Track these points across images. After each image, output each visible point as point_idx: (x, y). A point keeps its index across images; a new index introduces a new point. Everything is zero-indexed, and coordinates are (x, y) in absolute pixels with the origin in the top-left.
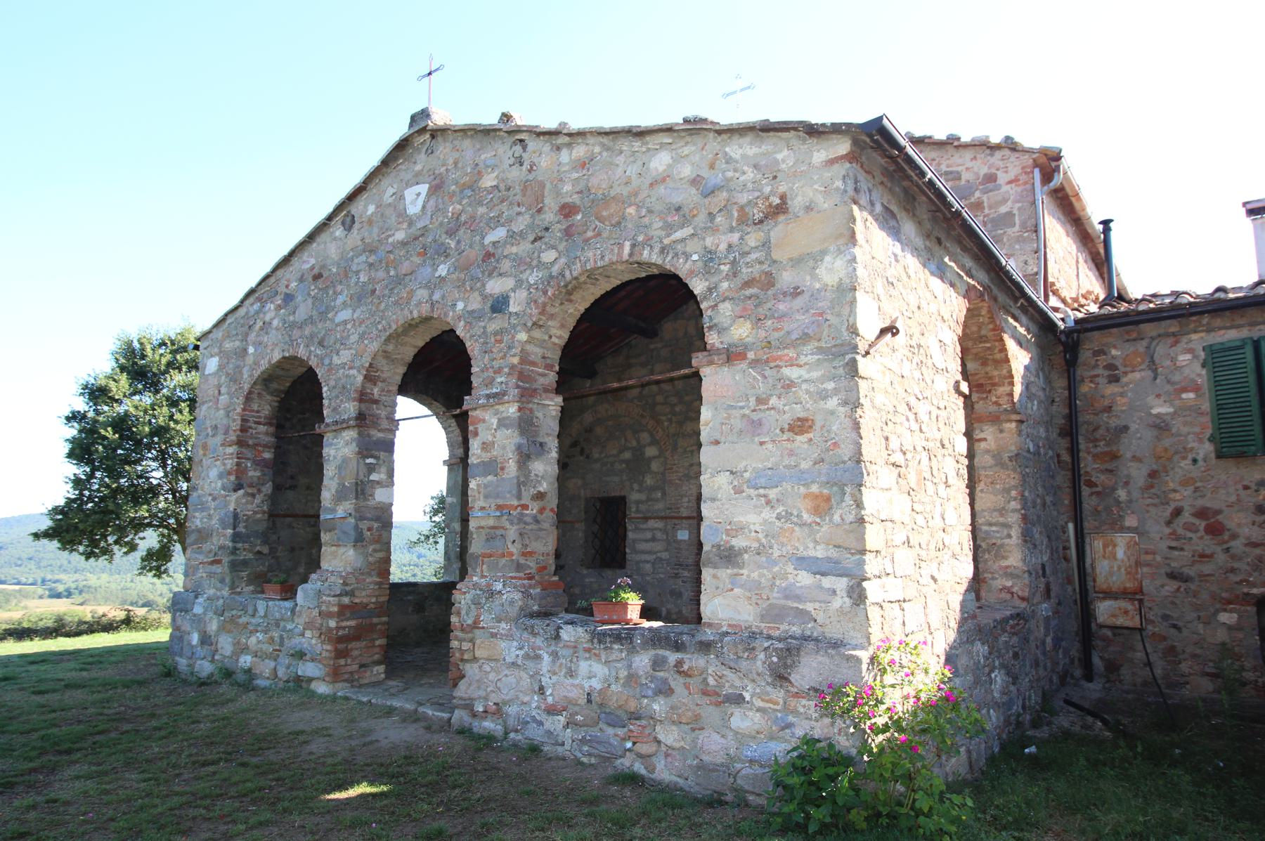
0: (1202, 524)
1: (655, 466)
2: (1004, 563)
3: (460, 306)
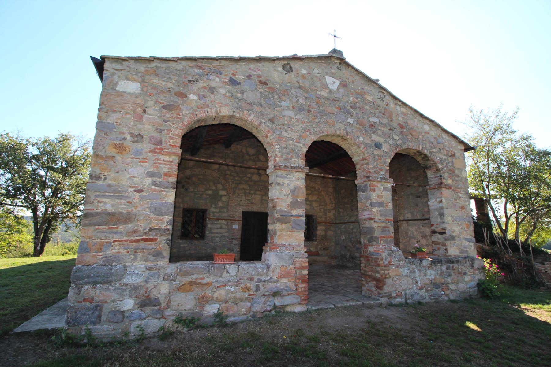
1: (224, 199)
3: (361, 139)
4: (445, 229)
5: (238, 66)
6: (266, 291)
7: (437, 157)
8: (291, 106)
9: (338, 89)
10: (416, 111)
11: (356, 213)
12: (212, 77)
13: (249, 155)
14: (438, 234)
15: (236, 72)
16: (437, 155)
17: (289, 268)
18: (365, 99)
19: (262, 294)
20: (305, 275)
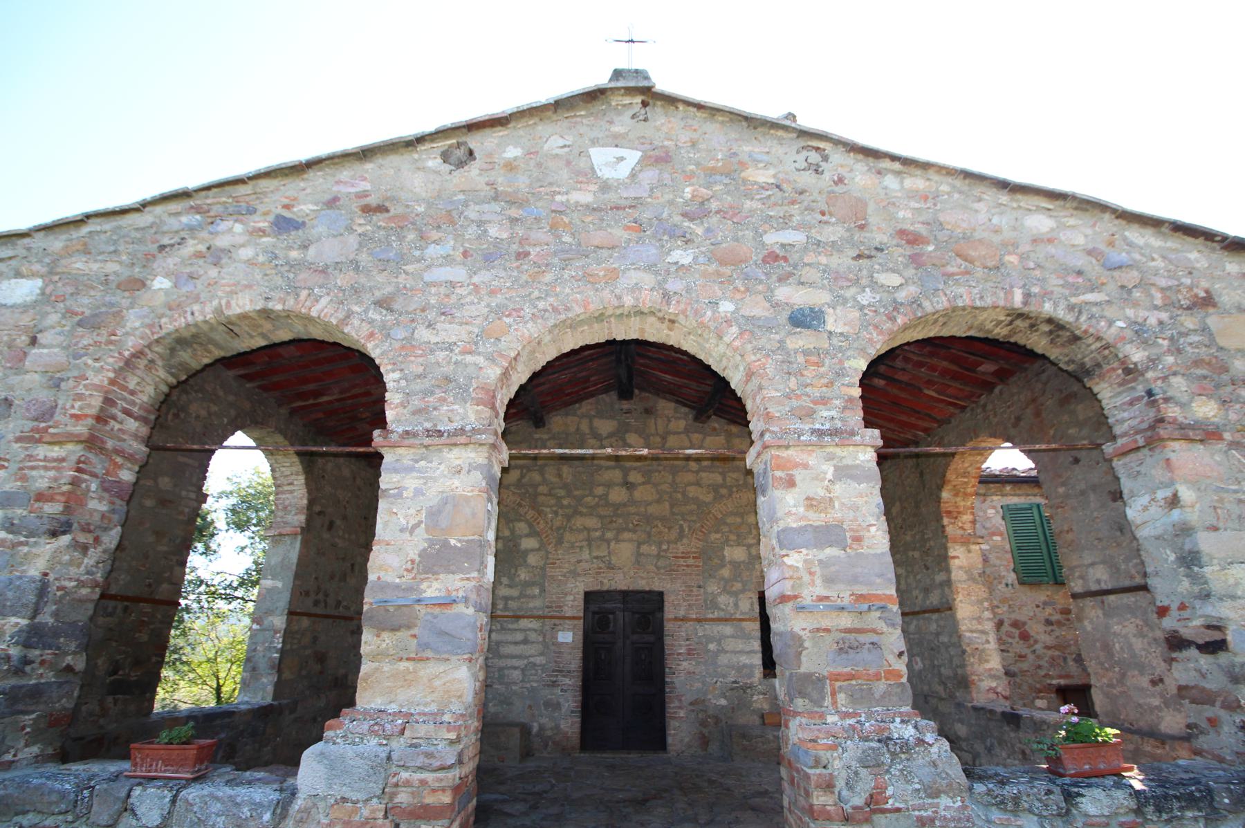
0: (1016, 632)
1: (532, 559)
2: (988, 666)
3: (726, 307)
4: (1218, 628)
5: (302, 184)
7: (1111, 321)
8: (458, 255)
9: (633, 175)
10: (967, 175)
11: (940, 577)
12: (223, 226)
14: (1193, 652)
15: (295, 199)
16: (1109, 312)
17: (366, 812)
18: (745, 181)
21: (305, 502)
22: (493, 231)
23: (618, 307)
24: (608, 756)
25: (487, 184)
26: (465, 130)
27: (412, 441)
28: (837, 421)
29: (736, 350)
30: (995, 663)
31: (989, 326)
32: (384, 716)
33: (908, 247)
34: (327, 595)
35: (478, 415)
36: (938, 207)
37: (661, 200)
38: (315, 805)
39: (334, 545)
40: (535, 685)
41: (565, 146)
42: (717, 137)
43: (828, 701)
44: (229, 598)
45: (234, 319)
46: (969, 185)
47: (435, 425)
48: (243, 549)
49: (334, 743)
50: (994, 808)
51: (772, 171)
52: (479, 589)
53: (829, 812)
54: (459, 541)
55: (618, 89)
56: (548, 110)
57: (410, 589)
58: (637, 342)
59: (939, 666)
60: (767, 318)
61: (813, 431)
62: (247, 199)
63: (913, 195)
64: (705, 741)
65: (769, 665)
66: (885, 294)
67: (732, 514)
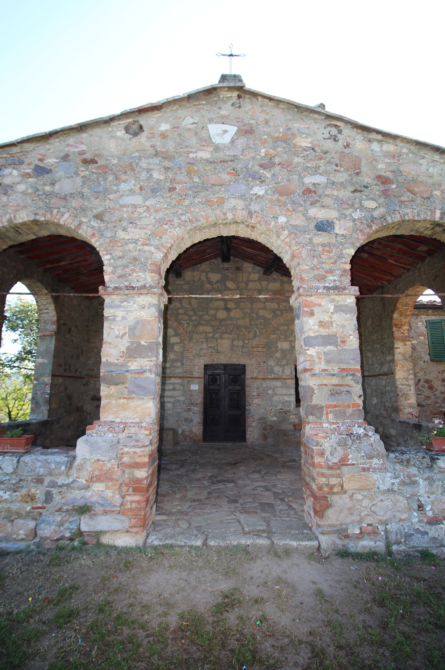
0: (427, 385)
1: (176, 348)
3: (282, 220)
5: (48, 146)
6: (65, 504)
9: (233, 141)
13: (210, 283)
15: (45, 155)
17: (109, 465)
18: (294, 145)
19: (57, 508)
20: (142, 480)
21: (55, 318)
22: (156, 175)
23: (224, 220)
24: (217, 444)
25: (151, 146)
26: (137, 113)
27: (119, 292)
28: (337, 282)
29: (286, 243)
30: (413, 400)
31: (422, 230)
32: (114, 424)
33: (381, 186)
34: (70, 366)
35: (152, 278)
36: (400, 162)
37: (248, 157)
38: (85, 463)
39: (72, 341)
40: (179, 410)
41: (194, 123)
42: (279, 117)
43: (324, 417)
44: (11, 367)
45: (18, 225)
46: (418, 149)
47: (130, 284)
48: (16, 341)
49: (92, 436)
50: (397, 464)
51: (310, 140)
52: (156, 365)
53: (321, 465)
54: (146, 342)
55: (224, 87)
56: (184, 101)
57: (123, 366)
58: (233, 237)
59: (385, 402)
60: (304, 226)
61: (325, 287)
62: (18, 155)
63: (387, 154)
64: (265, 437)
65: (298, 401)
66: (368, 213)
67: (282, 324)
